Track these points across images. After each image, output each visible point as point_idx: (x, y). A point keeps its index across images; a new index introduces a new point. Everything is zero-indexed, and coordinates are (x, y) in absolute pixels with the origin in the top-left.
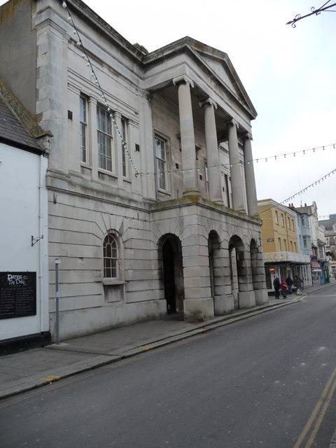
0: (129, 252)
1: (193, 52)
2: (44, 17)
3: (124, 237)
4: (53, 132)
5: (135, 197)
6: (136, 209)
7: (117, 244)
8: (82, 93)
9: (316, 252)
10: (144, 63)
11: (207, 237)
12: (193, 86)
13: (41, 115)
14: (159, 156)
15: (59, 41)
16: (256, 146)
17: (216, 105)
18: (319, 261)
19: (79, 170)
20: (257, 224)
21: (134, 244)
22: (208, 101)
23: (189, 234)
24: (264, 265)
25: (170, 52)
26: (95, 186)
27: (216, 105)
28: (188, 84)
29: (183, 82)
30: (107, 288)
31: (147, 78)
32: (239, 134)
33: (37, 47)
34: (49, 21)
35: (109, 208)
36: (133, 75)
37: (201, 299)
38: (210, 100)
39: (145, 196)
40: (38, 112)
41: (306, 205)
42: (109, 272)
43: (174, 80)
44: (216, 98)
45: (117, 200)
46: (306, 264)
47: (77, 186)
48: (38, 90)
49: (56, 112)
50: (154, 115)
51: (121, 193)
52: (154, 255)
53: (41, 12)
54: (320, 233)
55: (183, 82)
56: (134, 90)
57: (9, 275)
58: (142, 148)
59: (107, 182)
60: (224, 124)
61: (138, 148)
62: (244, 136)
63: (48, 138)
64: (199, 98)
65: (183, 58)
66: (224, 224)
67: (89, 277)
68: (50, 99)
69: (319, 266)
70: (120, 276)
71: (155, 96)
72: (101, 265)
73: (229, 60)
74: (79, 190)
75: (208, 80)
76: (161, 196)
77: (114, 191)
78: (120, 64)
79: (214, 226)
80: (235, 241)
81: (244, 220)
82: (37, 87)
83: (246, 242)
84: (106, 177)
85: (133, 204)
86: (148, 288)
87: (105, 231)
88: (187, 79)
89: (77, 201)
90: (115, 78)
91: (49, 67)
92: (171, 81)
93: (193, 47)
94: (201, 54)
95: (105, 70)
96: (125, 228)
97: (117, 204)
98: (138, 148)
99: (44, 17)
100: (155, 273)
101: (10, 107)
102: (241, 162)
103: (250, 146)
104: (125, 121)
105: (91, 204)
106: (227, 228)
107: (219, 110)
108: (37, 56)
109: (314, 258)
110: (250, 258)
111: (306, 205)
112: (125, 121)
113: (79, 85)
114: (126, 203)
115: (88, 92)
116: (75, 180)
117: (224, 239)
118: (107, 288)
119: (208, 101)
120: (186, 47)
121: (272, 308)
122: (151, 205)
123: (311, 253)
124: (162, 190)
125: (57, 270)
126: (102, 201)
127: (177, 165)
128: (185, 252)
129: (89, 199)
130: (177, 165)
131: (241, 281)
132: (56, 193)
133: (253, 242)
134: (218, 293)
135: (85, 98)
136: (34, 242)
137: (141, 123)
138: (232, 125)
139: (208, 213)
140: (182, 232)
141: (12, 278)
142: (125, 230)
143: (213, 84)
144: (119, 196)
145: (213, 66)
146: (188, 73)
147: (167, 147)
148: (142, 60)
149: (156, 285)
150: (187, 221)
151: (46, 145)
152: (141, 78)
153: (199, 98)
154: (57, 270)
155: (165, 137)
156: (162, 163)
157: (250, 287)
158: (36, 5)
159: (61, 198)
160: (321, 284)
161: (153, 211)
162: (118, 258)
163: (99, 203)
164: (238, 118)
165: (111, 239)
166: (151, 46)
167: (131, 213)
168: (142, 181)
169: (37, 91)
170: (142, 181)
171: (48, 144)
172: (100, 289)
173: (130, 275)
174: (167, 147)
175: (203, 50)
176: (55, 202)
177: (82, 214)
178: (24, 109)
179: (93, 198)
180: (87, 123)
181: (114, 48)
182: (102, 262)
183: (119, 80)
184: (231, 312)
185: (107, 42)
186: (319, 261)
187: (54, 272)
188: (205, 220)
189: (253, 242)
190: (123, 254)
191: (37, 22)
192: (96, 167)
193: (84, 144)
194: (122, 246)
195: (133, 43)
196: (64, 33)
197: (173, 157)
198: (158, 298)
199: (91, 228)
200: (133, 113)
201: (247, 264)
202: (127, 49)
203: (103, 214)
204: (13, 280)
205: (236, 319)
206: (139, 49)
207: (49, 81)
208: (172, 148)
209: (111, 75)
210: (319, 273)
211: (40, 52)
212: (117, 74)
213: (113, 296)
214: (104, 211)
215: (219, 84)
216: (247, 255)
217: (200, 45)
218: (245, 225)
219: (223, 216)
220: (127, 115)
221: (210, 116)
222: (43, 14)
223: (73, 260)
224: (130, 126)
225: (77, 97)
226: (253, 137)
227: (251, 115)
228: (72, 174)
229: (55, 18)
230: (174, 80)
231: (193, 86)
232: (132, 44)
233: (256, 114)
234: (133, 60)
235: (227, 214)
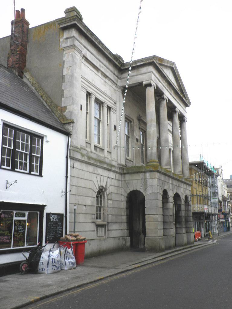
0: (110, 202)
1: (157, 65)
2: (69, 43)
3: (108, 192)
4: (75, 121)
5: (114, 163)
6: (114, 172)
7: (102, 196)
8: (87, 92)
9: (221, 205)
10: (122, 68)
11: (162, 194)
12: (156, 88)
13: (65, 108)
14: (127, 133)
15: (78, 57)
16: (188, 125)
17: (179, 112)
18: (223, 213)
19: (84, 145)
20: (189, 185)
21: (113, 197)
22: (163, 96)
23: (151, 192)
24: (192, 215)
25: (141, 63)
26: (93, 156)
27: (179, 112)
28: (153, 87)
29: (150, 85)
30: (98, 226)
31: (123, 78)
32: (168, 107)
33: (64, 61)
34: (73, 47)
35: (100, 171)
36: (115, 76)
37: (158, 237)
38: (177, 110)
39: (119, 162)
40: (63, 105)
41: (214, 167)
42: (98, 217)
43: (144, 83)
44: (168, 95)
45: (105, 166)
46: (214, 215)
47: (85, 156)
48: (64, 90)
49: (75, 106)
50: (125, 105)
51: (107, 161)
52: (124, 205)
53: (67, 39)
54: (224, 190)
55: (150, 85)
56: (114, 87)
57: (51, 215)
58: (118, 128)
59: (98, 153)
60: (172, 110)
61: (115, 128)
62: (182, 119)
63: (72, 124)
64: (159, 94)
65: (151, 69)
66: (171, 185)
67: (89, 219)
68: (73, 98)
69: (223, 217)
70: (104, 218)
71: (84, 58)
72: (94, 210)
73: (176, 67)
74: (85, 159)
75: (163, 82)
76: (128, 162)
77: (102, 159)
78: (108, 70)
79: (165, 186)
80: (177, 197)
81: (182, 182)
82: (63, 88)
83: (183, 197)
84: (98, 149)
85: (113, 169)
86: (119, 229)
87: (98, 187)
88: (153, 83)
89: (84, 167)
90: (104, 79)
91: (72, 76)
92: (141, 83)
93: (157, 61)
94: (160, 64)
95: (100, 74)
96: (108, 185)
97: (105, 169)
98: (115, 128)
99: (69, 43)
100: (124, 218)
101: (42, 100)
102: (170, 131)
103: (185, 125)
104: (109, 108)
105: (91, 168)
106: (173, 188)
107: (169, 103)
108: (63, 67)
109: (220, 210)
110: (184, 209)
111: (214, 167)
112: (109, 108)
113: (86, 86)
114: (109, 168)
115: (90, 91)
116: (84, 152)
117: (171, 194)
118: (98, 226)
119: (163, 96)
120: (153, 62)
121: (199, 246)
122: (123, 169)
123: (218, 206)
124: (128, 158)
125: (75, 213)
126: (97, 166)
127: (137, 139)
128: (147, 204)
129: (90, 165)
130: (137, 139)
131: (178, 226)
132: (74, 161)
133: (186, 198)
134: (179, 232)
135: (89, 95)
136: (8, 185)
137: (118, 110)
138: (176, 112)
139: (163, 177)
140: (145, 190)
141: (52, 217)
142: (108, 187)
143: (166, 84)
144: (106, 163)
145: (168, 73)
146: (153, 79)
147: (131, 126)
148: (121, 66)
149: (124, 226)
150: (149, 182)
151: (70, 128)
152: (119, 78)
153: (159, 94)
154: (75, 213)
155: (131, 120)
156: (128, 137)
157: (184, 230)
158: (63, 34)
159: (77, 165)
160: (224, 232)
161: (124, 174)
162: (103, 206)
163: (95, 168)
164: (179, 107)
165: (101, 192)
166: (127, 58)
167: (112, 175)
168: (117, 152)
169: (63, 91)
170: (117, 152)
171: (72, 128)
172: (93, 227)
173: (110, 218)
174: (131, 126)
175: (162, 62)
176: (73, 167)
177: (87, 175)
178: (52, 102)
179: (93, 165)
180: (102, 119)
181: (105, 59)
182: (95, 208)
183: (107, 81)
184: (186, 245)
185: (93, 47)
186: (223, 213)
187: (73, 214)
188: (161, 182)
189: (186, 198)
190: (108, 203)
191: (64, 45)
192: (95, 142)
193: (86, 129)
194: (106, 198)
195: (114, 53)
196: (80, 52)
197: (135, 134)
198: (126, 235)
199: (90, 185)
200: (113, 103)
201: (183, 213)
202: (113, 59)
203: (97, 175)
204: (53, 218)
205: (177, 253)
206: (117, 58)
207: (72, 85)
208: (135, 127)
209: (102, 77)
210: (222, 222)
211: (66, 65)
212: (97, 69)
213: (101, 231)
214: (97, 173)
215: (170, 84)
216: (183, 207)
217: (161, 59)
218: (183, 186)
219: (171, 180)
220: (110, 105)
221: (164, 105)
222: (69, 40)
223: (81, 206)
224: (112, 113)
225: (85, 95)
226: (187, 120)
227: (186, 104)
228: (82, 148)
229: (77, 43)
230: (144, 83)
231: (156, 88)
232: (114, 54)
233: (190, 103)
234: (115, 66)
235: (173, 178)
